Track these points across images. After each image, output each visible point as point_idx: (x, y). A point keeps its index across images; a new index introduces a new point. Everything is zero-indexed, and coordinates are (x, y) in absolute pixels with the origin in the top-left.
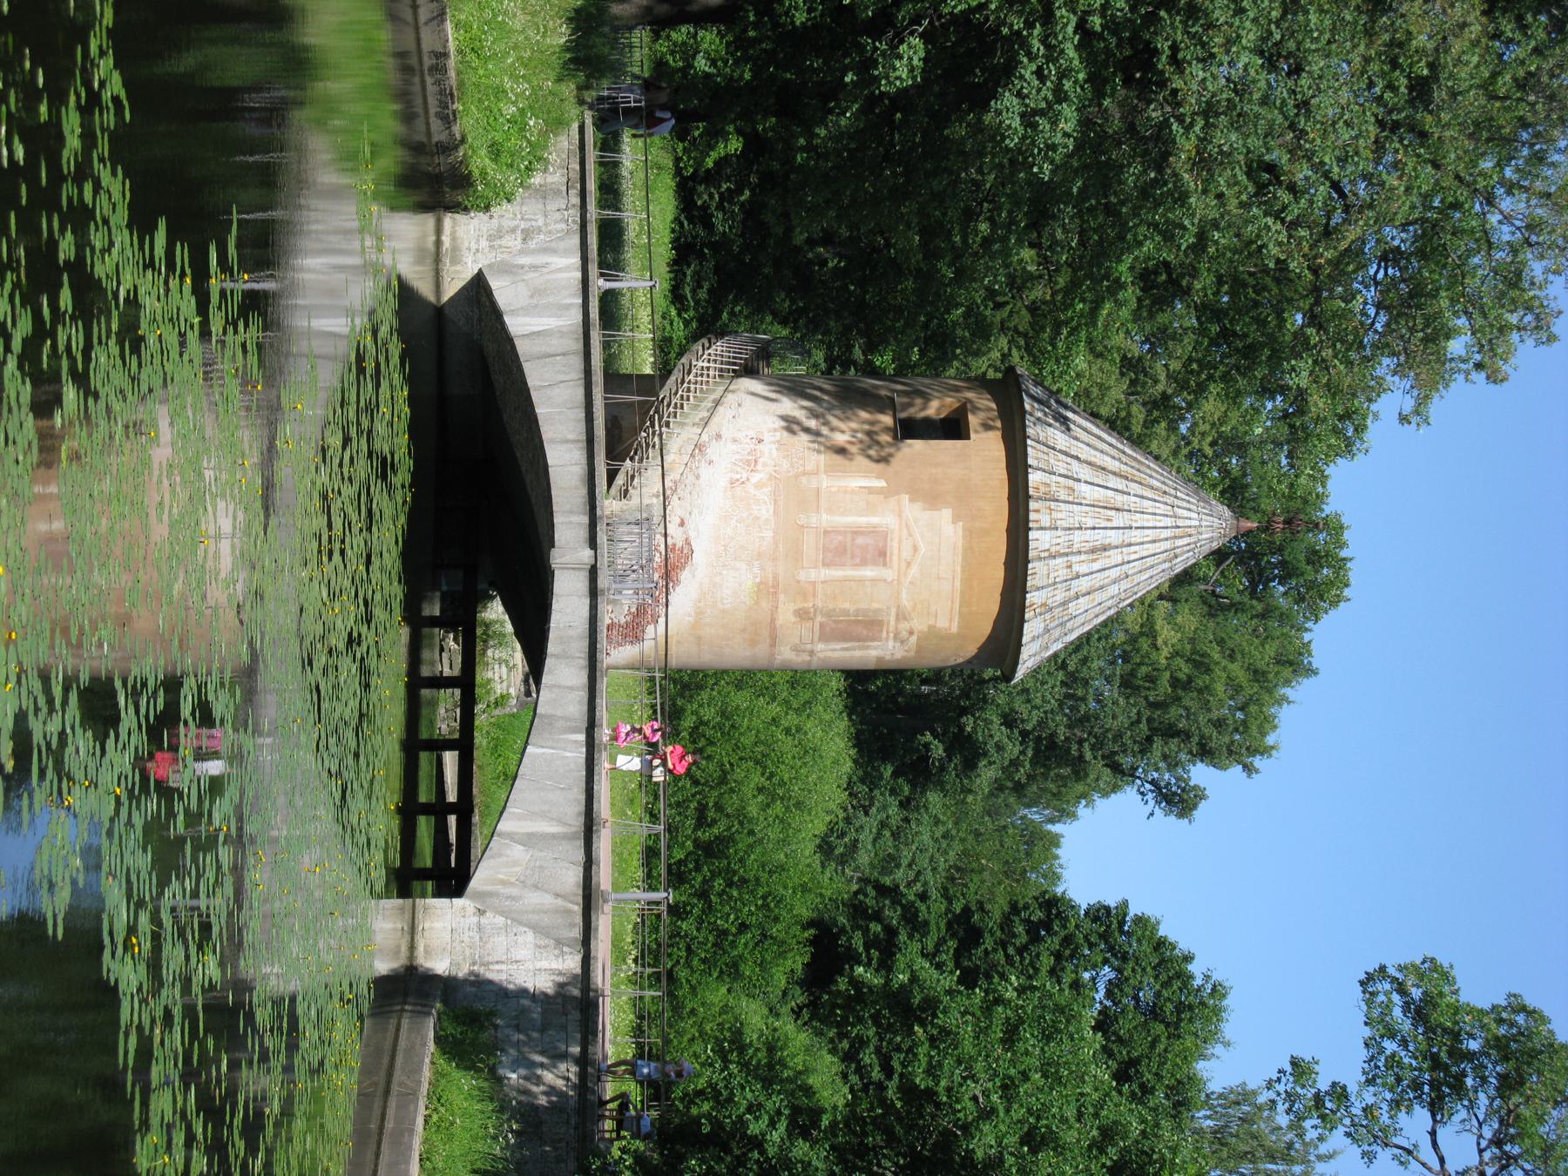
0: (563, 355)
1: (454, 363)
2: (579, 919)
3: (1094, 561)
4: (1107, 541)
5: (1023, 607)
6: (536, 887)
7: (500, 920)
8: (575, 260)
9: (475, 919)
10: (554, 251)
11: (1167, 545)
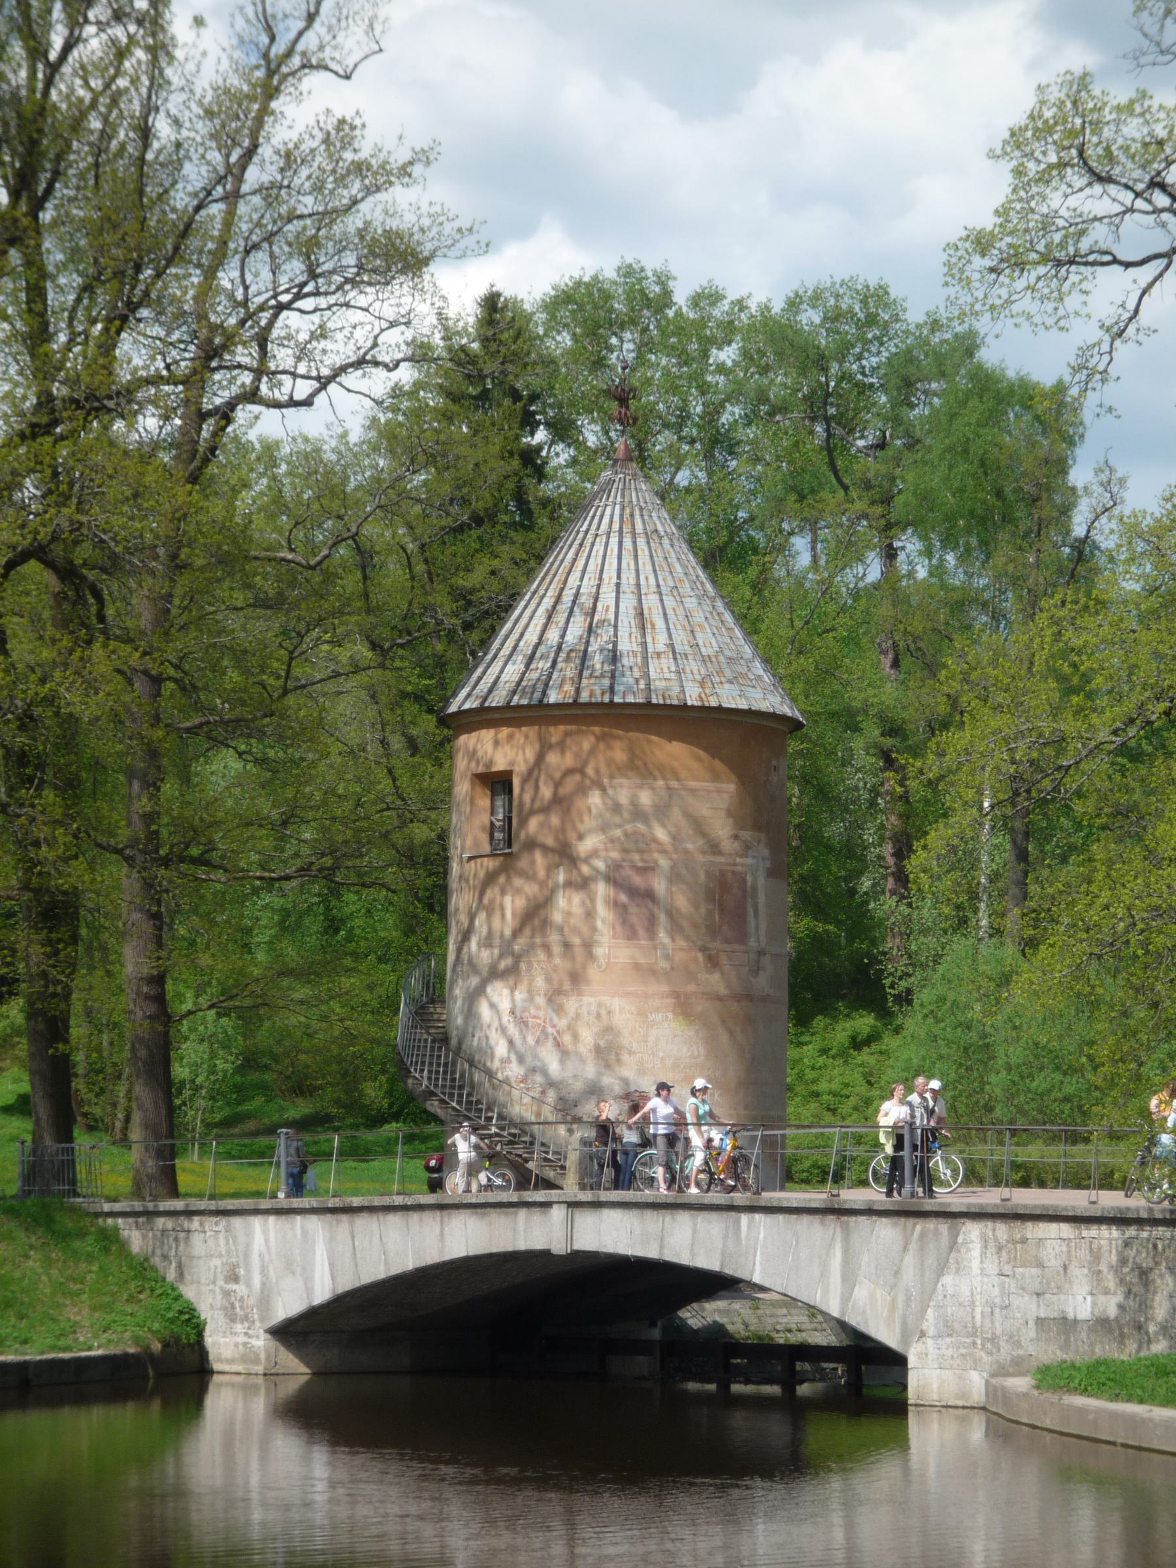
0: (353, 1237)
1: (392, 1369)
2: (931, 1224)
3: (653, 626)
4: (632, 611)
5: (703, 709)
6: (897, 1273)
7: (930, 1314)
8: (256, 1222)
9: (930, 1342)
10: (248, 1246)
11: (641, 542)
